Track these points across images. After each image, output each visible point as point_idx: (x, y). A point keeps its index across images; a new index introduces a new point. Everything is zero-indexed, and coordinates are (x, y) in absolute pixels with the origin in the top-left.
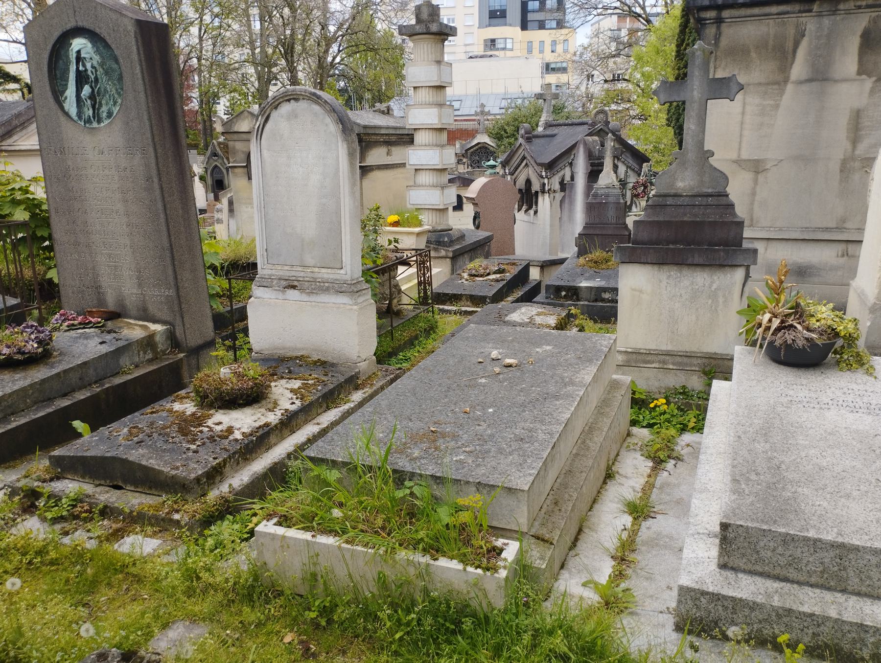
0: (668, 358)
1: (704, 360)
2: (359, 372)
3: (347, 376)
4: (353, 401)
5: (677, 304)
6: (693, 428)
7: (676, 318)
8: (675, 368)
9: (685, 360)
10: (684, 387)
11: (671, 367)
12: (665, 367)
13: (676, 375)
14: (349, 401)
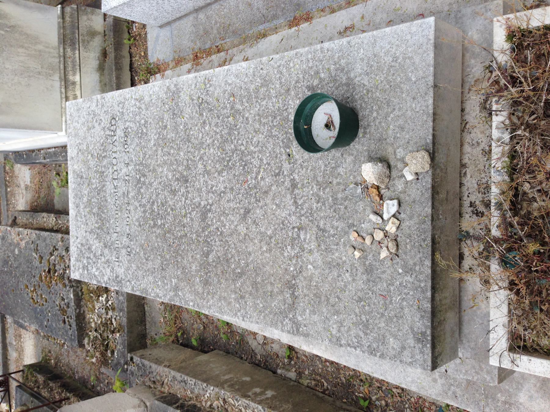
5: (7, 66)
7: (23, 68)
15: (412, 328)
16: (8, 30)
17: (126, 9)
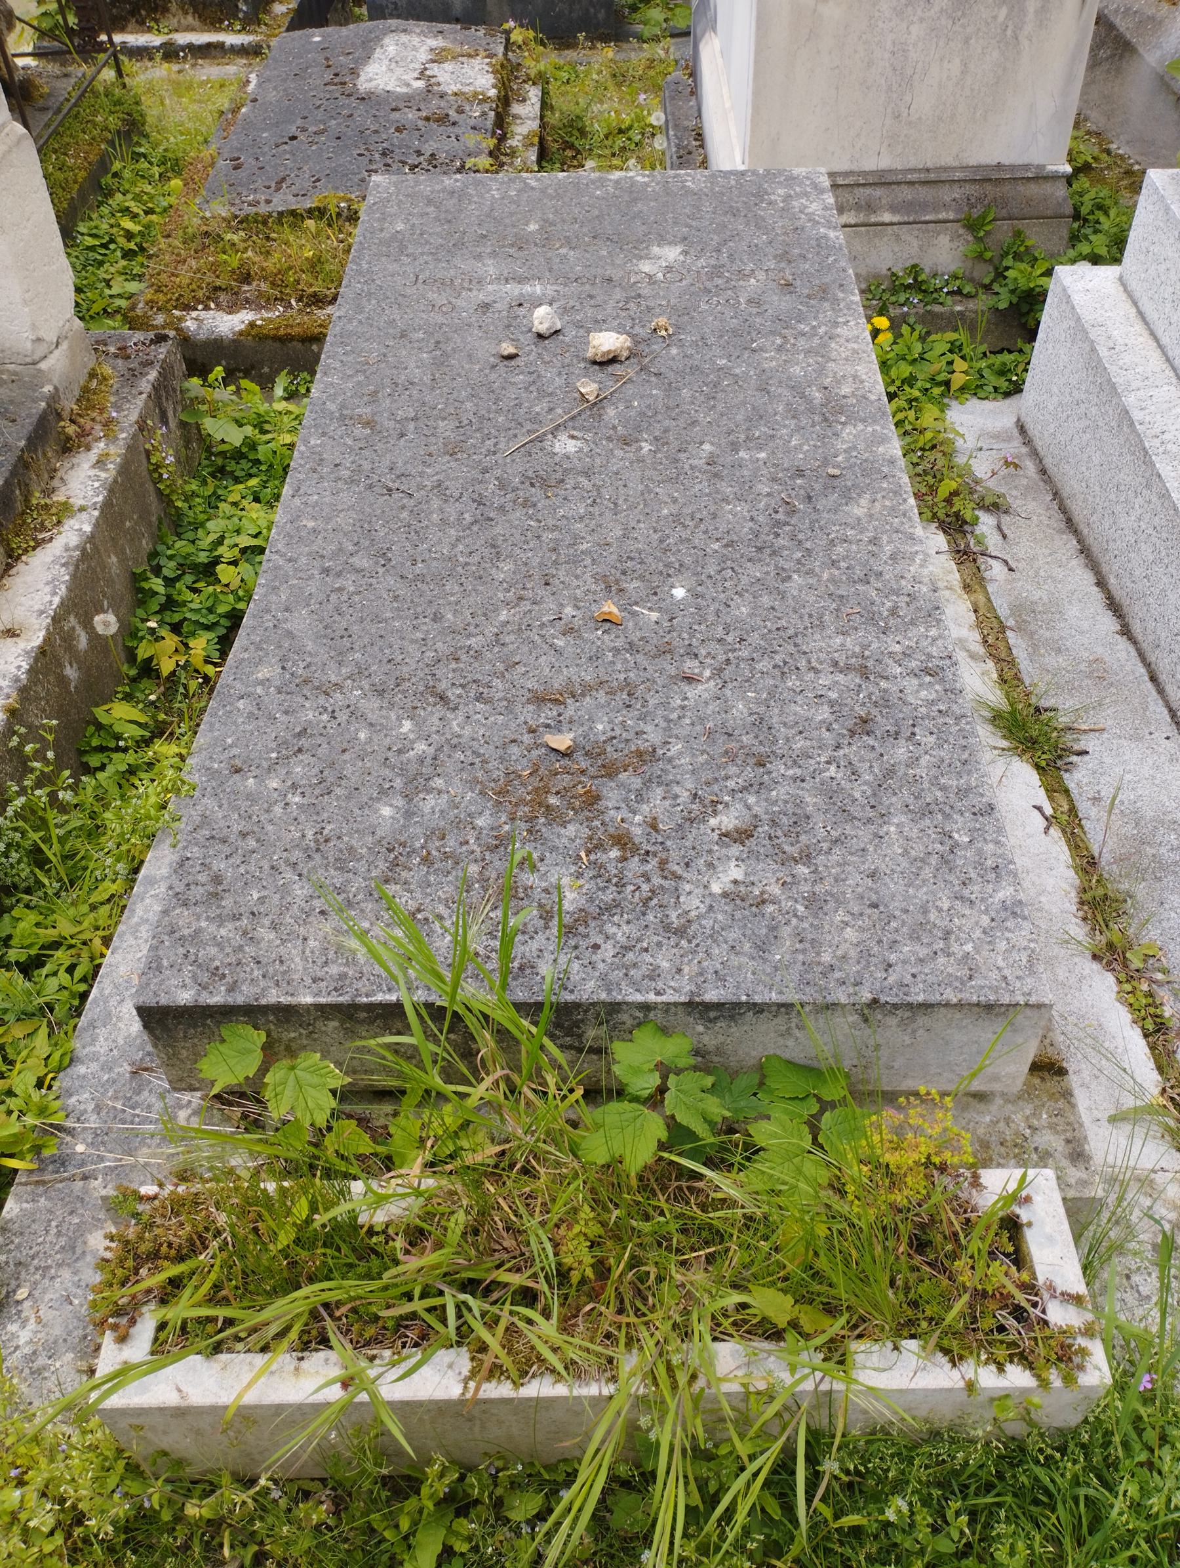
0: (878, 192)
1: (969, 189)
2: (54, 398)
3: (28, 424)
4: (82, 509)
5: (914, 29)
6: (962, 389)
7: (909, 72)
8: (896, 219)
9: (924, 193)
10: (915, 270)
11: (887, 217)
12: (873, 219)
13: (898, 238)
14: (66, 509)
15: (79, 1371)
16: (1009, 32)
17: (1065, 325)
